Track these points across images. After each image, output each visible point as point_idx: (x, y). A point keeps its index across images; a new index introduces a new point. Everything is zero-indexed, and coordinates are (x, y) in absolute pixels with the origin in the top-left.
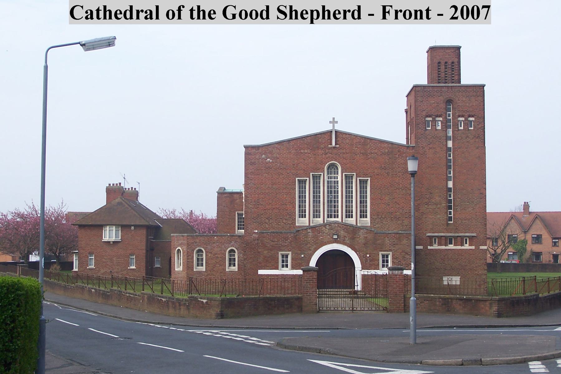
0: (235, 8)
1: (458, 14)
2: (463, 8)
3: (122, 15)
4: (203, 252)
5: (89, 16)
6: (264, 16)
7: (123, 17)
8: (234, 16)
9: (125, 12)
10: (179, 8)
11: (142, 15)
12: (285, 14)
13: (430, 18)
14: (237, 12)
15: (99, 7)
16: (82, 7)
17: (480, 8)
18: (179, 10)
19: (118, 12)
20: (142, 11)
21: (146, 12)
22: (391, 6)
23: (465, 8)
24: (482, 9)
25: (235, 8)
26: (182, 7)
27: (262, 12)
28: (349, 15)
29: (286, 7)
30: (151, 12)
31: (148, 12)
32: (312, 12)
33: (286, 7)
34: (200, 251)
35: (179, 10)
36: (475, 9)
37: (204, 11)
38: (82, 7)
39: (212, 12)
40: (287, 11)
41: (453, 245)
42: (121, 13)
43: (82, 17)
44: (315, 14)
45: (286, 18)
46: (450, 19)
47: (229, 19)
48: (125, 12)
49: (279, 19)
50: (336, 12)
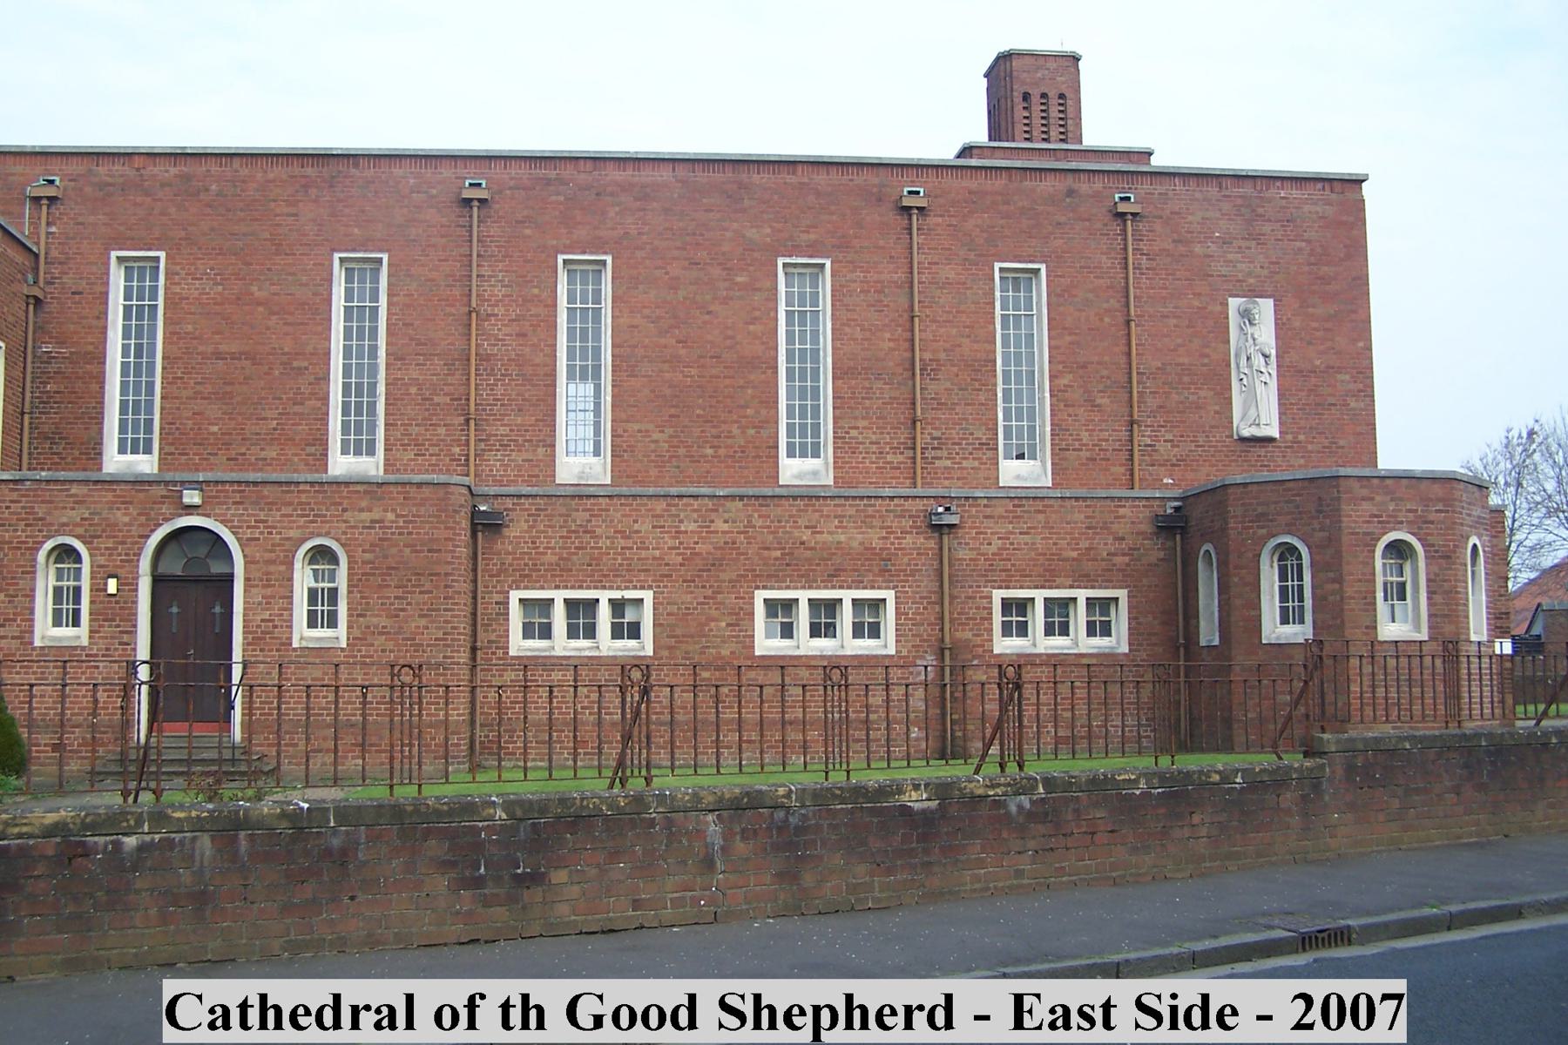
0: (602, 1001)
1: (1315, 1014)
2: (1327, 999)
3: (312, 1019)
4: (78, 559)
5: (220, 1020)
6: (683, 1018)
7: (314, 1024)
8: (598, 1021)
9: (320, 1011)
10: (472, 999)
11: (367, 1019)
12: (741, 1016)
13: (1112, 1025)
14: (607, 1011)
15: (247, 998)
16: (200, 997)
17: (1377, 999)
18: (472, 1005)
19: (301, 1011)
20: (368, 1008)
21: (378, 1011)
22: (1038, 996)
23: (1334, 1002)
24: (1381, 1001)
25: (602, 1001)
26: (477, 996)
27: (675, 1011)
28: (920, 1018)
29: (742, 997)
30: (392, 1010)
31: (385, 1011)
32: (817, 1010)
33: (742, 997)
34: (66, 554)
35: (472, 1005)
36: (1363, 1002)
37: (864, 1010)
38: (200, 997)
39: (1228, 1011)
40: (748, 1009)
41: (55, 583)
42: (308, 1013)
43: (200, 1025)
44: (825, 1016)
45: (743, 1024)
46: (1292, 1029)
47: (584, 1029)
48: (320, 1011)
49: (722, 1029)
50: (299, 1013)
